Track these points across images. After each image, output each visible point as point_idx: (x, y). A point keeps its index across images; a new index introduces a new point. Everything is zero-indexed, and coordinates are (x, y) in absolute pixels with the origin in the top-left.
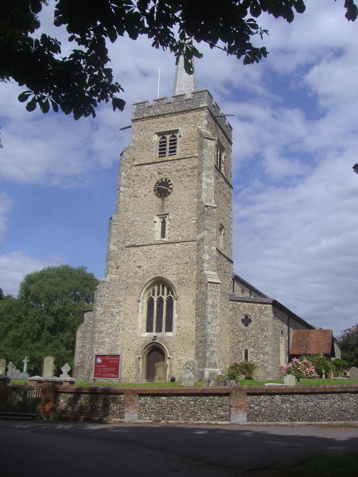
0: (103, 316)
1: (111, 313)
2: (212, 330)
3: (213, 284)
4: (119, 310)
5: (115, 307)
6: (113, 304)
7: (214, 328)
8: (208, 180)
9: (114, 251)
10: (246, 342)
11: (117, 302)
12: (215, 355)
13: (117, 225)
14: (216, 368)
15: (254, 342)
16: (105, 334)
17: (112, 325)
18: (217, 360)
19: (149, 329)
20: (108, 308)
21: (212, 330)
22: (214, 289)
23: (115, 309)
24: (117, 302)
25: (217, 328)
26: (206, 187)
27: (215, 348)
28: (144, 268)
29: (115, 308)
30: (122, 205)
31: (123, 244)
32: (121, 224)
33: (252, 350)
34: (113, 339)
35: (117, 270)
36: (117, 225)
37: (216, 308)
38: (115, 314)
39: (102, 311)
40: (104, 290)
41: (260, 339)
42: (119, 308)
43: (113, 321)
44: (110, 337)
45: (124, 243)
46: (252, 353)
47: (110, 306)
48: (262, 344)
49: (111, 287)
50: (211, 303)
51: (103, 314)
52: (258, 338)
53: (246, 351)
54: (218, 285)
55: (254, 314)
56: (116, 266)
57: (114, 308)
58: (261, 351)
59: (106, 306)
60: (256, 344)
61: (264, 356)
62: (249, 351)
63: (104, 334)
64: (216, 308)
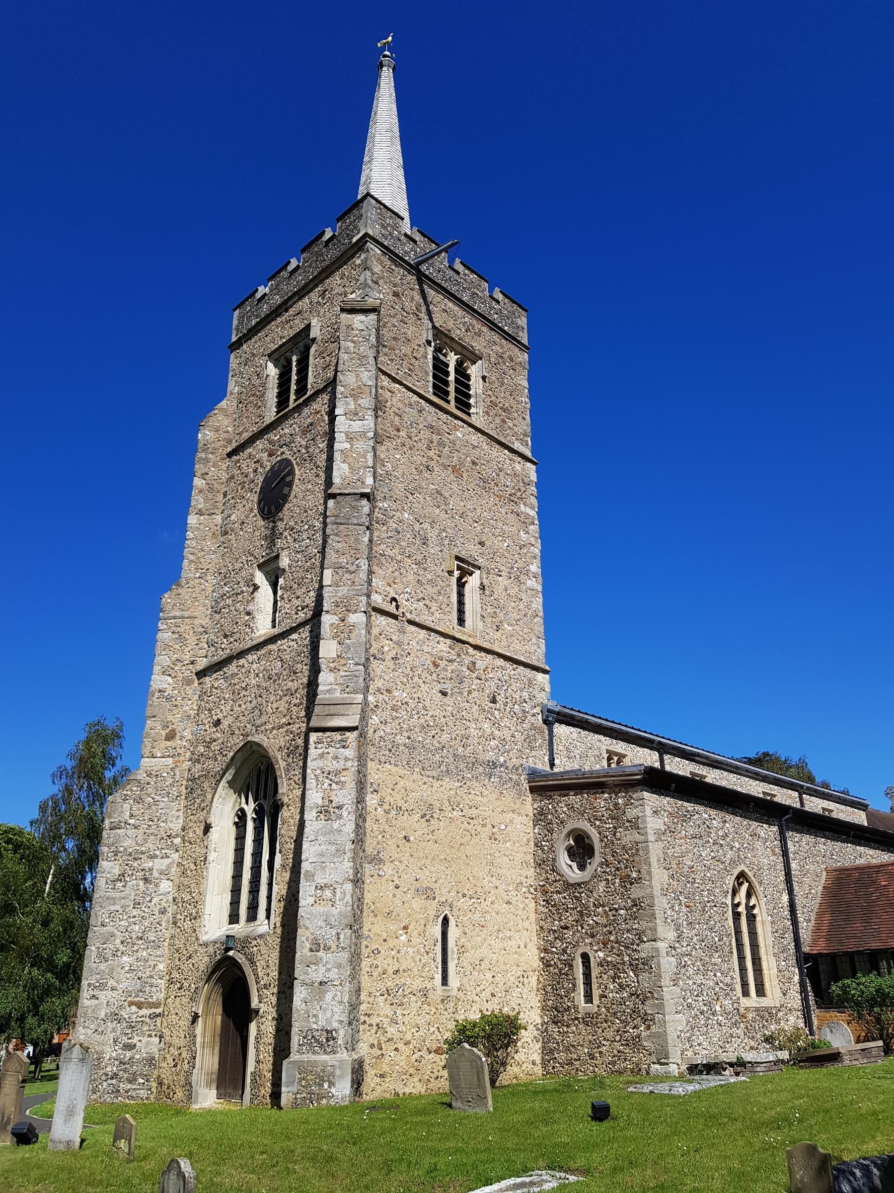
0: (119, 884)
1: (142, 873)
2: (318, 900)
3: (328, 734)
4: (170, 860)
5: (158, 853)
6: (151, 845)
7: (328, 893)
8: (357, 426)
9: (160, 691)
10: (583, 928)
11: (163, 838)
12: (329, 996)
13: (174, 618)
14: (334, 1052)
15: (606, 926)
16: (122, 942)
17: (146, 910)
18: (337, 1017)
19: (234, 918)
20: (135, 859)
21: (318, 900)
22: (330, 750)
23: (156, 860)
24: (163, 838)
25: (338, 891)
26: (348, 446)
27: (328, 970)
28: (225, 723)
29: (156, 856)
30: (191, 562)
31: (191, 667)
32: (186, 614)
33: (601, 954)
34: (144, 954)
35: (169, 743)
36: (174, 618)
37: (340, 817)
38: (156, 874)
39: (117, 871)
40: (125, 805)
41: (622, 912)
42: (167, 857)
43: (148, 899)
44: (136, 948)
45: (192, 663)
46: (601, 964)
47: (143, 853)
48: (628, 931)
49: (149, 795)
50: (320, 802)
51: (118, 880)
52: (617, 910)
53: (585, 957)
54: (348, 734)
55: (598, 823)
56: (168, 731)
57: (153, 857)
58: (626, 958)
59: (130, 854)
60: (610, 933)
61: (637, 976)
62: (592, 959)
63: (118, 941)
64: (340, 817)
